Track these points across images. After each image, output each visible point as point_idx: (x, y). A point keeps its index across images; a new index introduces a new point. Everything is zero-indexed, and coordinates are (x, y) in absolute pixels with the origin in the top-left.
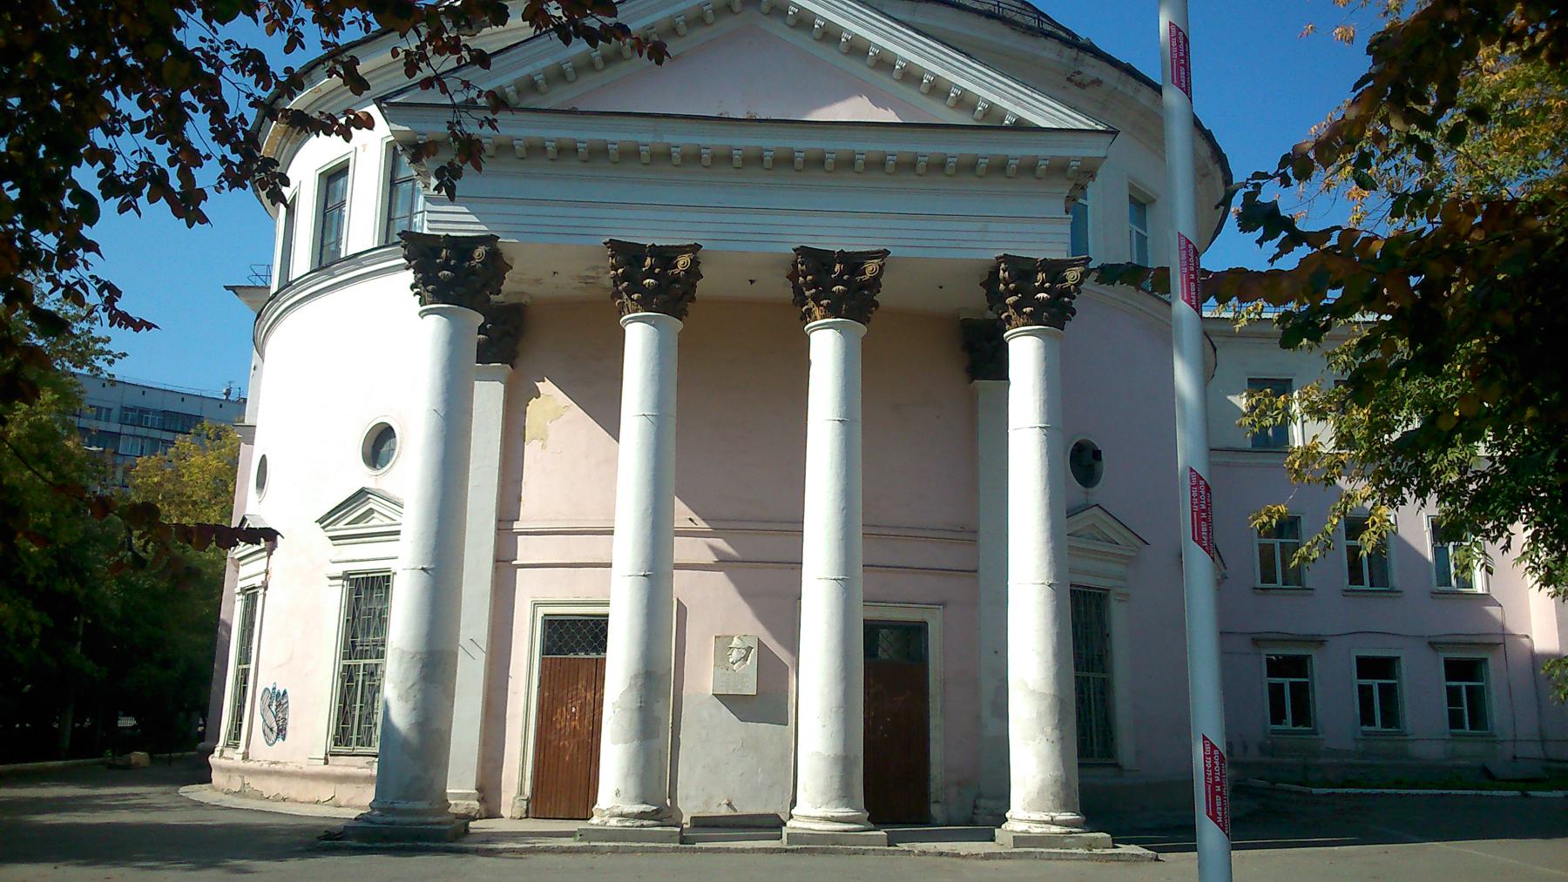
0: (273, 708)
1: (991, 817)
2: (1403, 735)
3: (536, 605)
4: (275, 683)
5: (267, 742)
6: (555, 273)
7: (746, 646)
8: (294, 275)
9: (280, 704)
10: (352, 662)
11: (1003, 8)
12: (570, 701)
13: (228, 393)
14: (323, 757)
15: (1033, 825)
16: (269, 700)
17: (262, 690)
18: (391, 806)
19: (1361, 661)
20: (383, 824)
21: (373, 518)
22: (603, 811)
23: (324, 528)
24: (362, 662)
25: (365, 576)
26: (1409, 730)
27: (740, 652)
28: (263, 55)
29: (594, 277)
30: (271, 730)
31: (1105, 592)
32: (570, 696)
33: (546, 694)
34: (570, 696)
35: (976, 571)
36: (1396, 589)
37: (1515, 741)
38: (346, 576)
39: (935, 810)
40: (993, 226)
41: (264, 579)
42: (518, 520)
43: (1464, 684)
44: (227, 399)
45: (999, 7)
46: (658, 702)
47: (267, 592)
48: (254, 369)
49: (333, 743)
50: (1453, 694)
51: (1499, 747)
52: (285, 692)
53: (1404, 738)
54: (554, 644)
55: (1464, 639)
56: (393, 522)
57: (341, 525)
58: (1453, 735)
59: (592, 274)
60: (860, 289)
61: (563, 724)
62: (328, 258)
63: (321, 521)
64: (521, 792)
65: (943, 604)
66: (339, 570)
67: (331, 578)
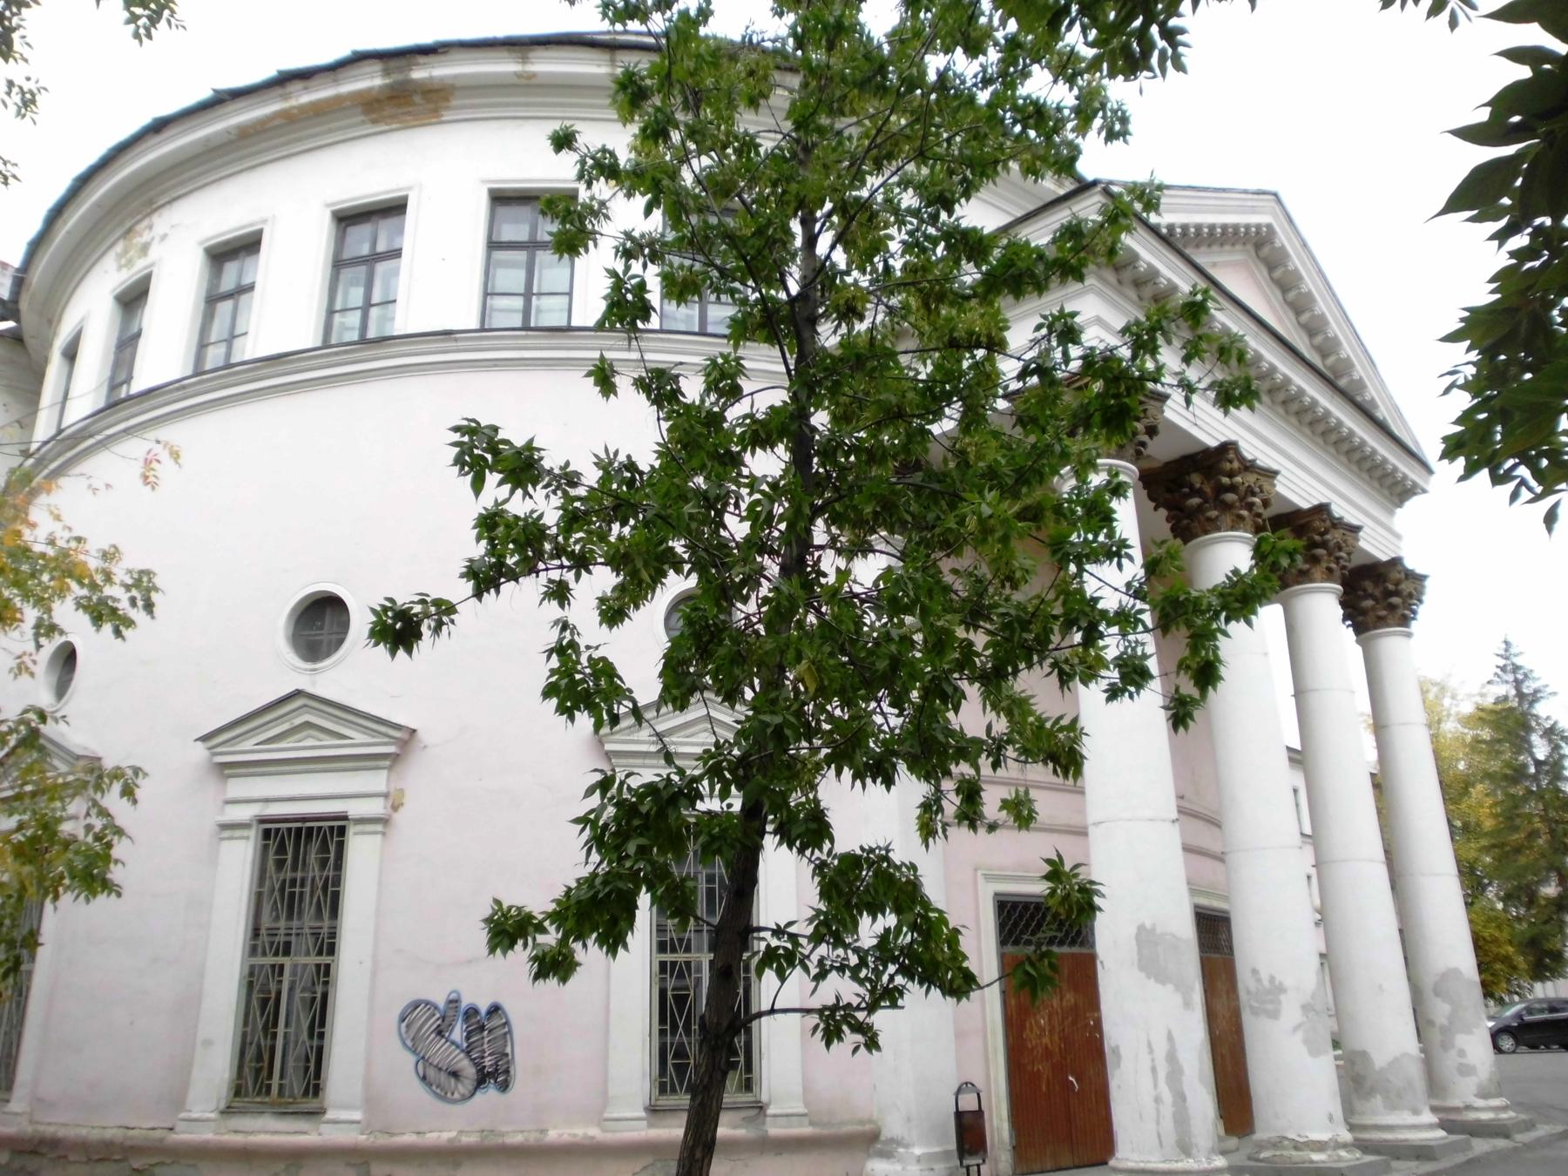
57: (248, 744)
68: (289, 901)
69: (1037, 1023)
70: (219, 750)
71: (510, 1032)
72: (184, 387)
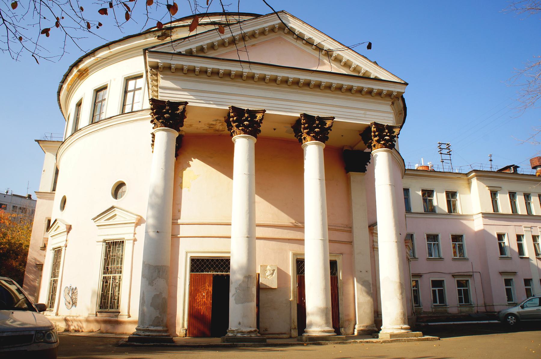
0: (70, 294)
2: (445, 306)
3: (187, 253)
6: (200, 122)
7: (273, 269)
8: (80, 127)
10: (107, 275)
12: (202, 291)
13: (7, 192)
14: (95, 313)
16: (68, 291)
18: (147, 328)
19: (433, 282)
21: (116, 218)
22: (234, 331)
23: (95, 222)
24: (112, 275)
25: (113, 241)
26: (447, 304)
27: (270, 272)
28: (102, 15)
29: (214, 125)
30: (69, 303)
32: (202, 289)
33: (192, 288)
34: (202, 289)
35: (352, 242)
36: (442, 258)
37: (478, 306)
38: (105, 241)
40: (368, 113)
41: (65, 243)
42: (180, 219)
43: (462, 288)
44: (7, 194)
46: (253, 287)
47: (66, 248)
48: (44, 171)
49: (99, 308)
50: (460, 291)
51: (473, 308)
52: (76, 288)
53: (446, 307)
54: (195, 268)
55: (462, 274)
56: (126, 219)
58: (460, 305)
59: (214, 123)
61: (199, 300)
62: (76, 130)
63: (94, 219)
64: (183, 327)
65: (342, 254)
67: (97, 242)
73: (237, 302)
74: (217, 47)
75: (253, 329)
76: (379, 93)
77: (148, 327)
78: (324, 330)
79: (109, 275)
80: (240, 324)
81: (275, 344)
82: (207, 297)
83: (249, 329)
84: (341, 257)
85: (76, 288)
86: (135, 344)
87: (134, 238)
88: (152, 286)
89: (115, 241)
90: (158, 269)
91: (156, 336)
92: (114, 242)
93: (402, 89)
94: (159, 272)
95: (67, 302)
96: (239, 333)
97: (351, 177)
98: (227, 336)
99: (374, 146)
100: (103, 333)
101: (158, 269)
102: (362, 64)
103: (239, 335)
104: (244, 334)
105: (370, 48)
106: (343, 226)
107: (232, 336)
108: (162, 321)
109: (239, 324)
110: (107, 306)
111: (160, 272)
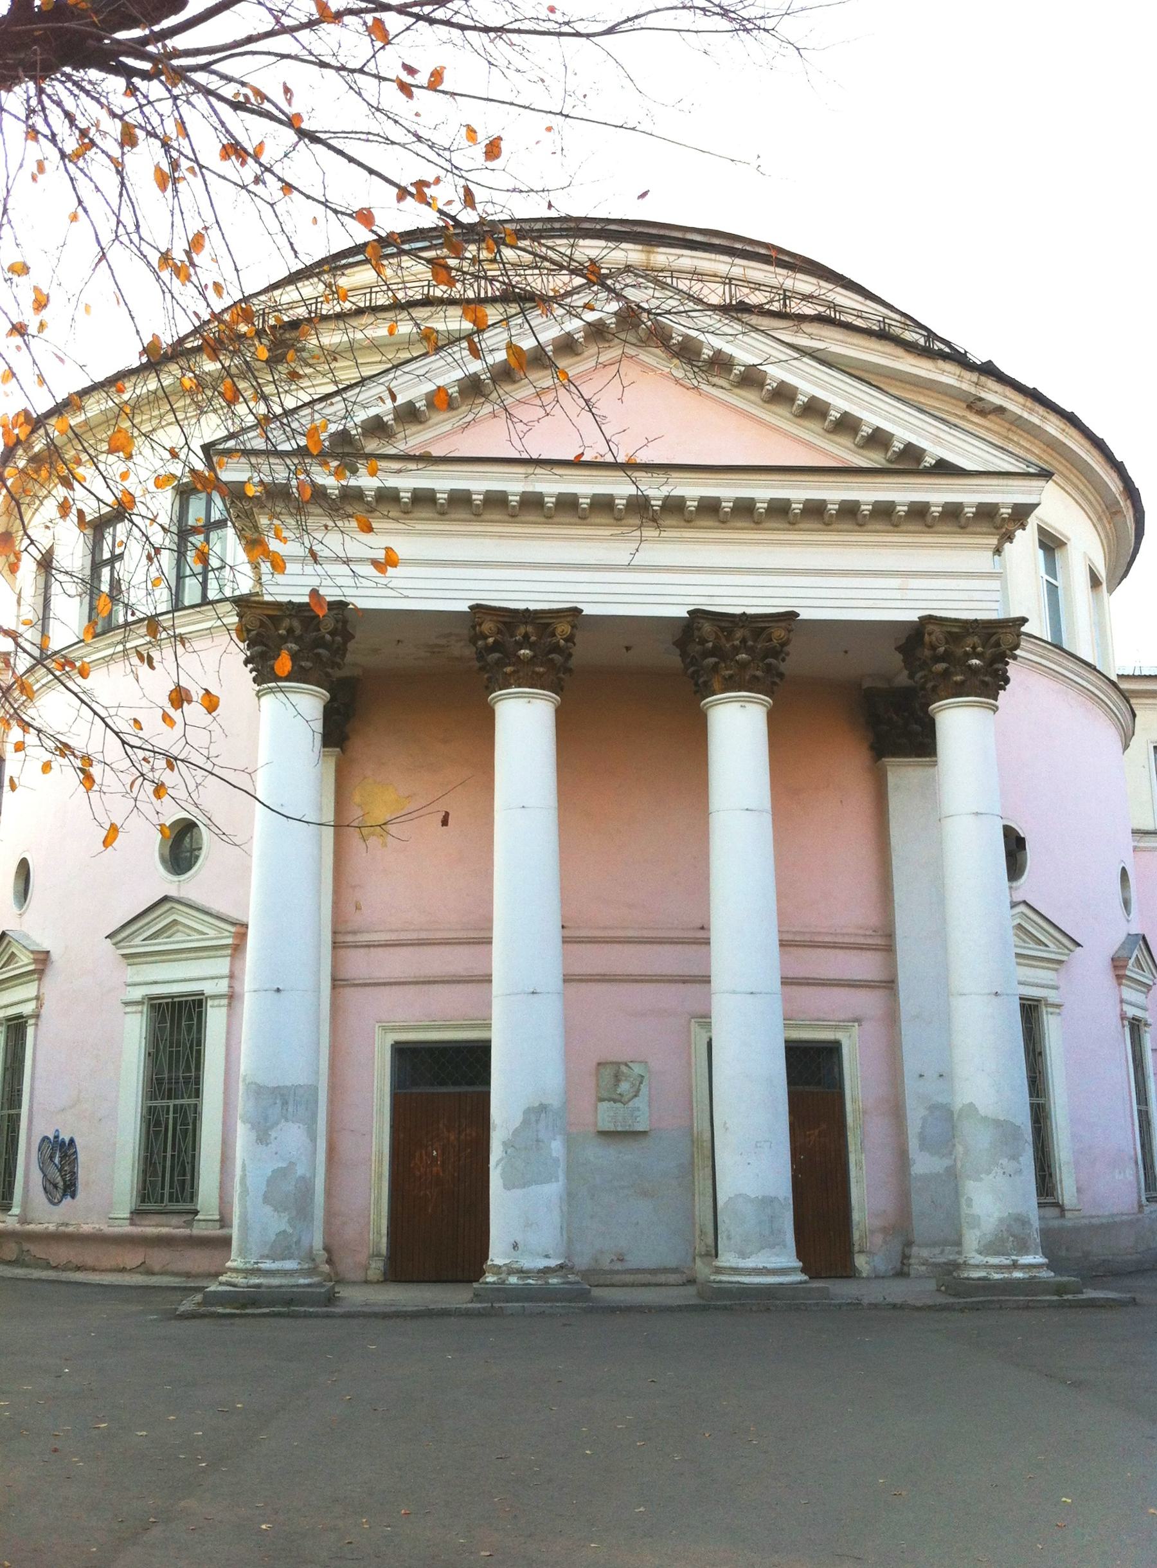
0: (57, 1160)
1: (924, 1268)
4: (57, 1130)
5: (49, 1200)
9: (66, 1155)
11: (889, 325)
15: (992, 1271)
17: (39, 1141)
18: (256, 1266)
20: (249, 1287)
22: (500, 1267)
24: (171, 1103)
25: (170, 1000)
29: (443, 646)
31: (1035, 1003)
39: (860, 1261)
45: (884, 323)
52: (72, 1141)
57: (138, 940)
59: (443, 642)
60: (550, 652)
65: (858, 1020)
66: (138, 993)
68: (174, 1059)
69: (429, 1155)
70: (122, 944)
71: (76, 1158)
72: (560, 617)
73: (508, 1186)
74: (326, 608)
75: (553, 1263)
76: (953, 513)
77: (257, 1263)
78: (765, 1265)
79: (165, 1102)
80: (515, 1246)
81: (613, 1307)
82: (443, 1162)
83: (542, 1263)
84: (856, 1029)
85: (72, 1141)
86: (220, 1310)
87: (231, 990)
88: (267, 1144)
89: (176, 1000)
90: (282, 1095)
91: (280, 1286)
92: (173, 1003)
93: (1030, 493)
94: (285, 1103)
95: (48, 1183)
96: (514, 1273)
97: (889, 773)
98: (483, 1283)
99: (934, 688)
100: (153, 1274)
101: (282, 1095)
102: (894, 422)
103: (513, 1280)
104: (529, 1278)
105: (447, 825)
106: (861, 932)
107: (494, 1283)
108: (298, 1242)
109: (514, 1248)
110: (163, 1194)
111: (287, 1103)
